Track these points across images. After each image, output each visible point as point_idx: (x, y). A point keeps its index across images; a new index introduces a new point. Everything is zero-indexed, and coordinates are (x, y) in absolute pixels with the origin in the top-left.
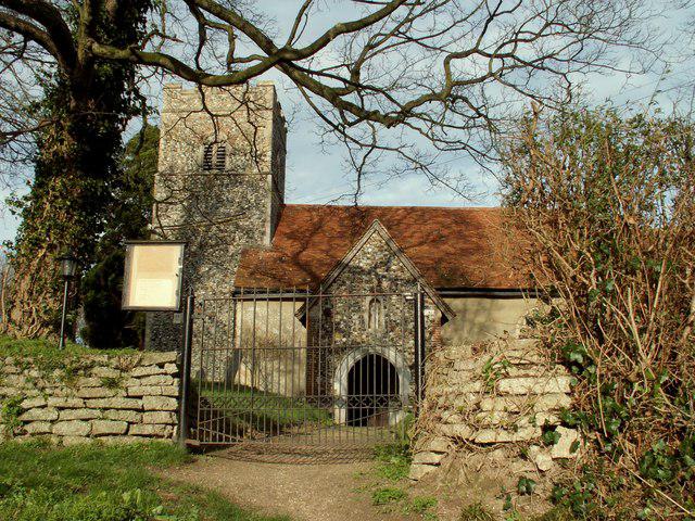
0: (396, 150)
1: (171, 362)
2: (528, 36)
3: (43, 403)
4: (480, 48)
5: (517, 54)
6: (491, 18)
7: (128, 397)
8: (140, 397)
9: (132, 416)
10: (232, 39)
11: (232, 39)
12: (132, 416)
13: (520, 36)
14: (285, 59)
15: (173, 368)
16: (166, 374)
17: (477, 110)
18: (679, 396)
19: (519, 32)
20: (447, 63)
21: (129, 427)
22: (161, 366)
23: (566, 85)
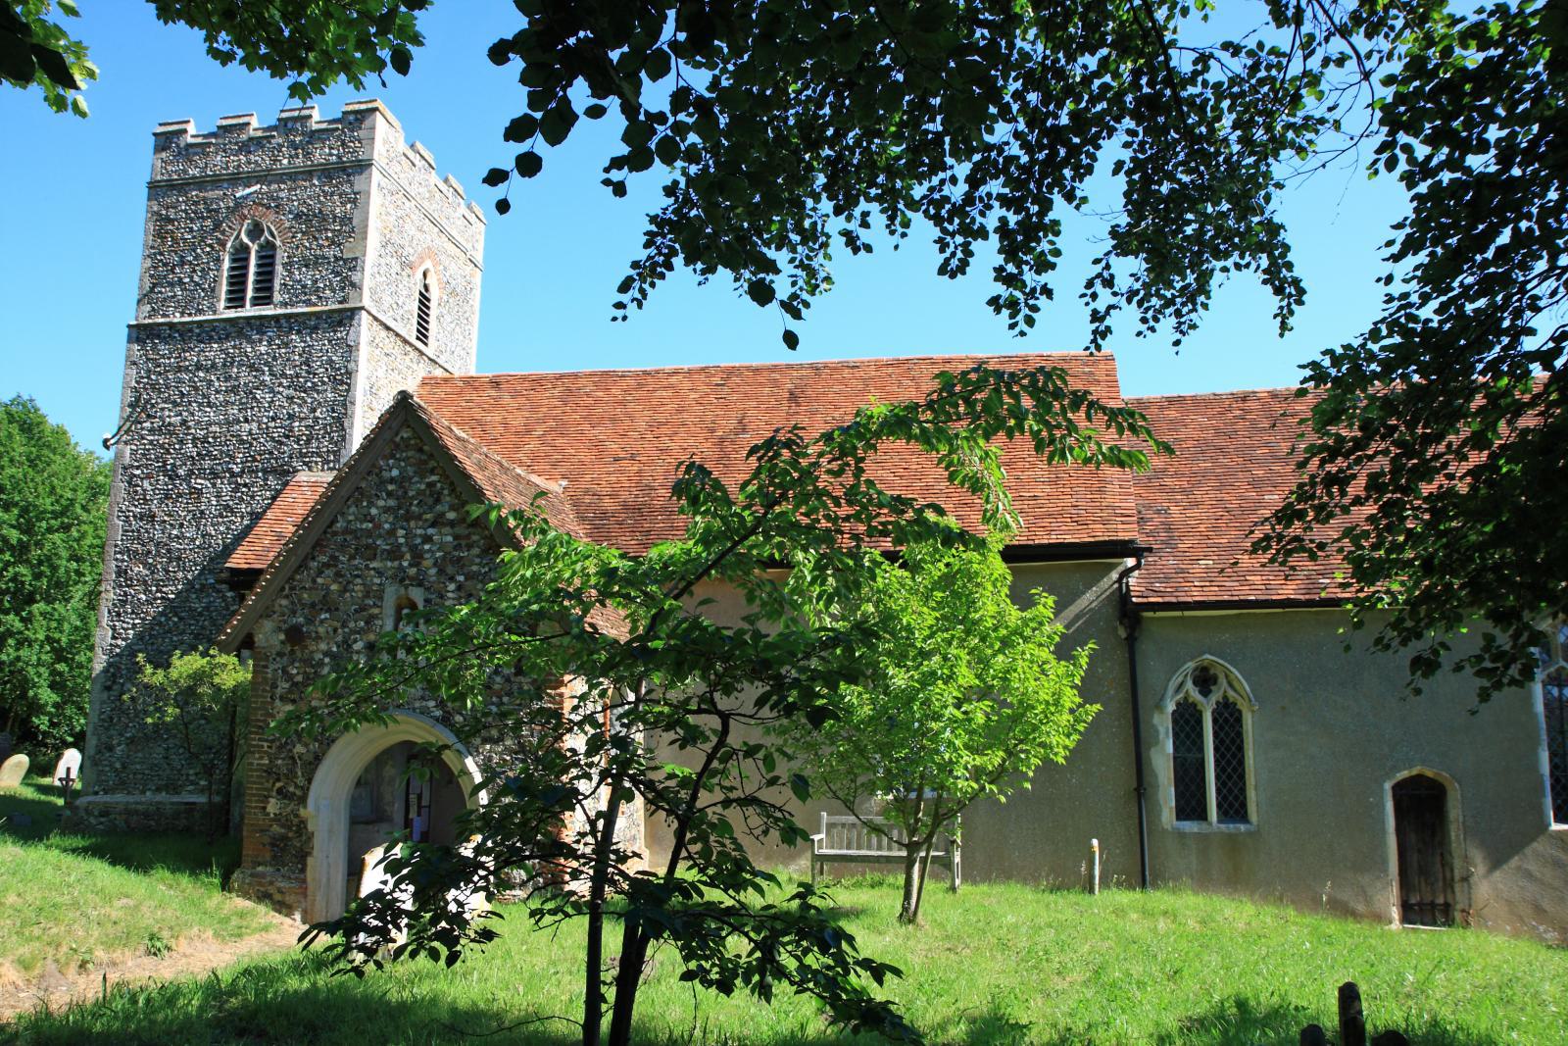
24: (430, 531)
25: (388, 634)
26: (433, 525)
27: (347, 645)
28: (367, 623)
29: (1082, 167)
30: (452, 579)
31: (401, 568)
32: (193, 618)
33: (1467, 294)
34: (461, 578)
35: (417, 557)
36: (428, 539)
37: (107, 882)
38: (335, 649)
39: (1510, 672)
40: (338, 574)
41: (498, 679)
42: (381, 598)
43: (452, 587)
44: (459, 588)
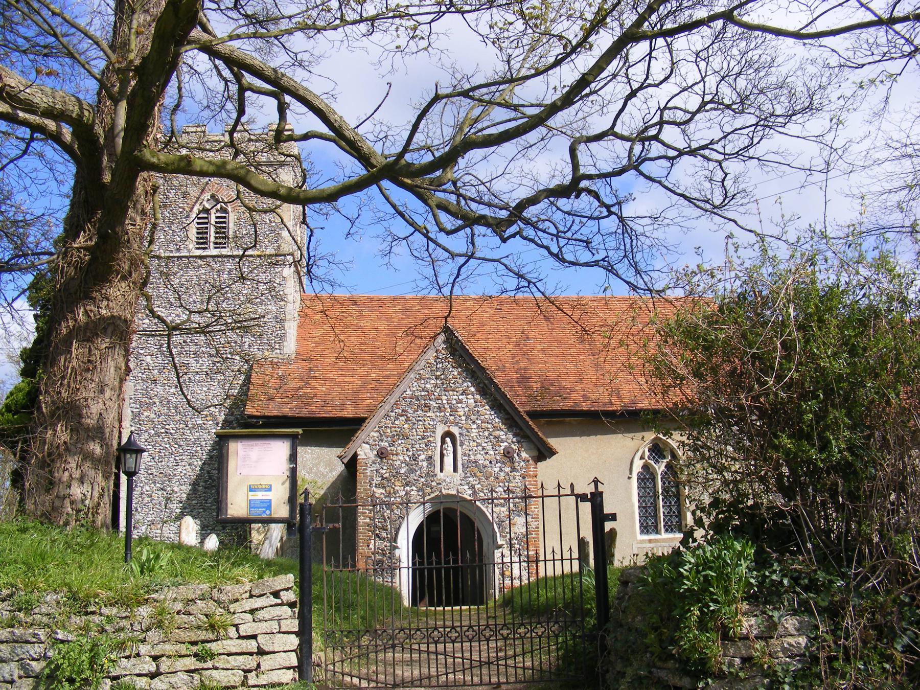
0: (498, 261)
1: (287, 589)
2: (680, 116)
3: (152, 668)
4: (617, 129)
5: (662, 137)
6: (633, 94)
7: (240, 637)
8: (254, 637)
9: (251, 662)
10: (282, 109)
11: (282, 109)
12: (251, 662)
13: (667, 115)
14: (483, 184)
15: (290, 596)
16: (282, 604)
17: (608, 207)
18: (500, 547)
19: (665, 108)
20: (573, 151)
21: (246, 677)
22: (276, 594)
23: (719, 175)
24: (461, 397)
25: (824, 431)
26: (462, 394)
27: (415, 458)
28: (426, 445)
29: (792, 578)
30: (474, 422)
31: (445, 416)
32: (188, 445)
33: (892, 368)
34: (479, 422)
35: (454, 410)
36: (460, 402)
37: (38, 650)
38: (408, 459)
39: (426, 357)
40: (408, 420)
41: (502, 474)
42: (434, 432)
43: (474, 426)
44: (478, 427)
